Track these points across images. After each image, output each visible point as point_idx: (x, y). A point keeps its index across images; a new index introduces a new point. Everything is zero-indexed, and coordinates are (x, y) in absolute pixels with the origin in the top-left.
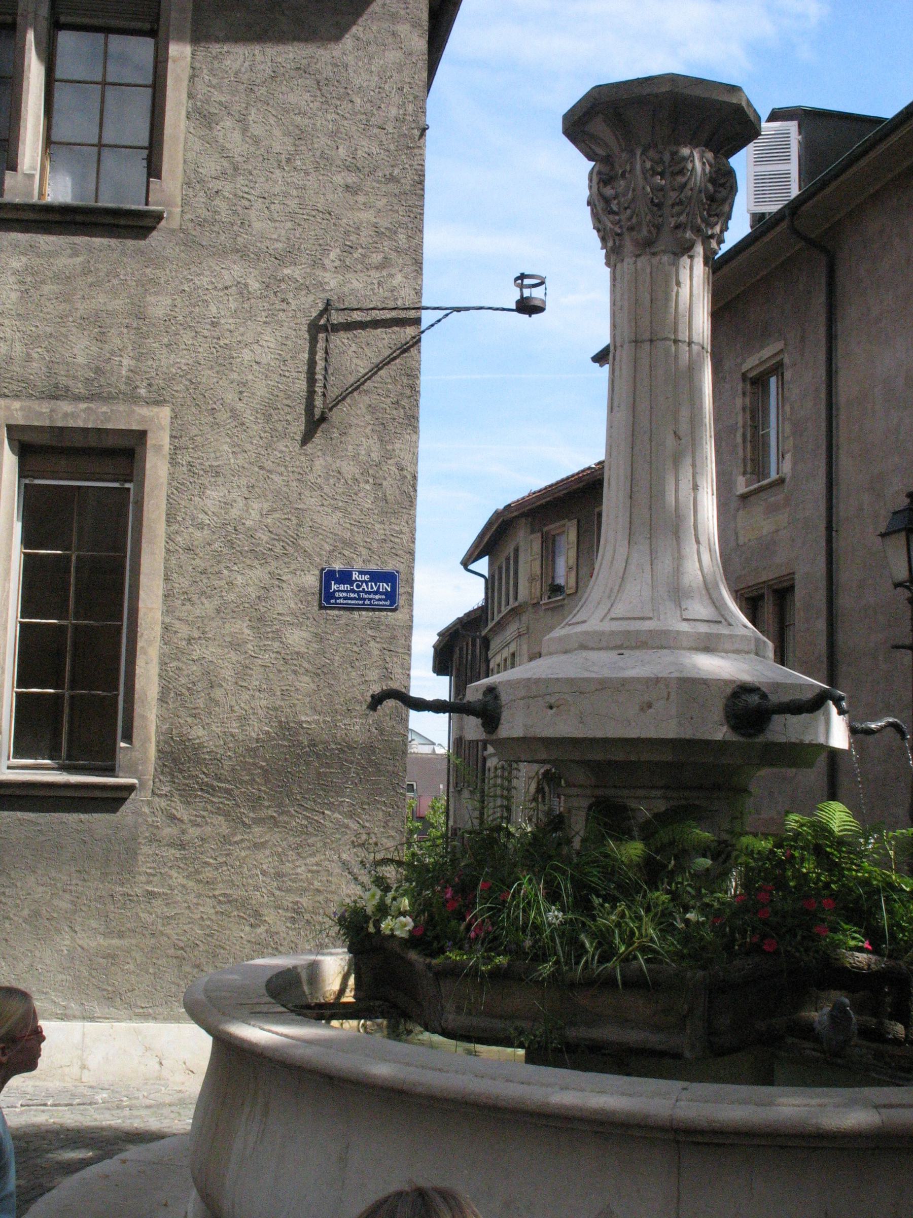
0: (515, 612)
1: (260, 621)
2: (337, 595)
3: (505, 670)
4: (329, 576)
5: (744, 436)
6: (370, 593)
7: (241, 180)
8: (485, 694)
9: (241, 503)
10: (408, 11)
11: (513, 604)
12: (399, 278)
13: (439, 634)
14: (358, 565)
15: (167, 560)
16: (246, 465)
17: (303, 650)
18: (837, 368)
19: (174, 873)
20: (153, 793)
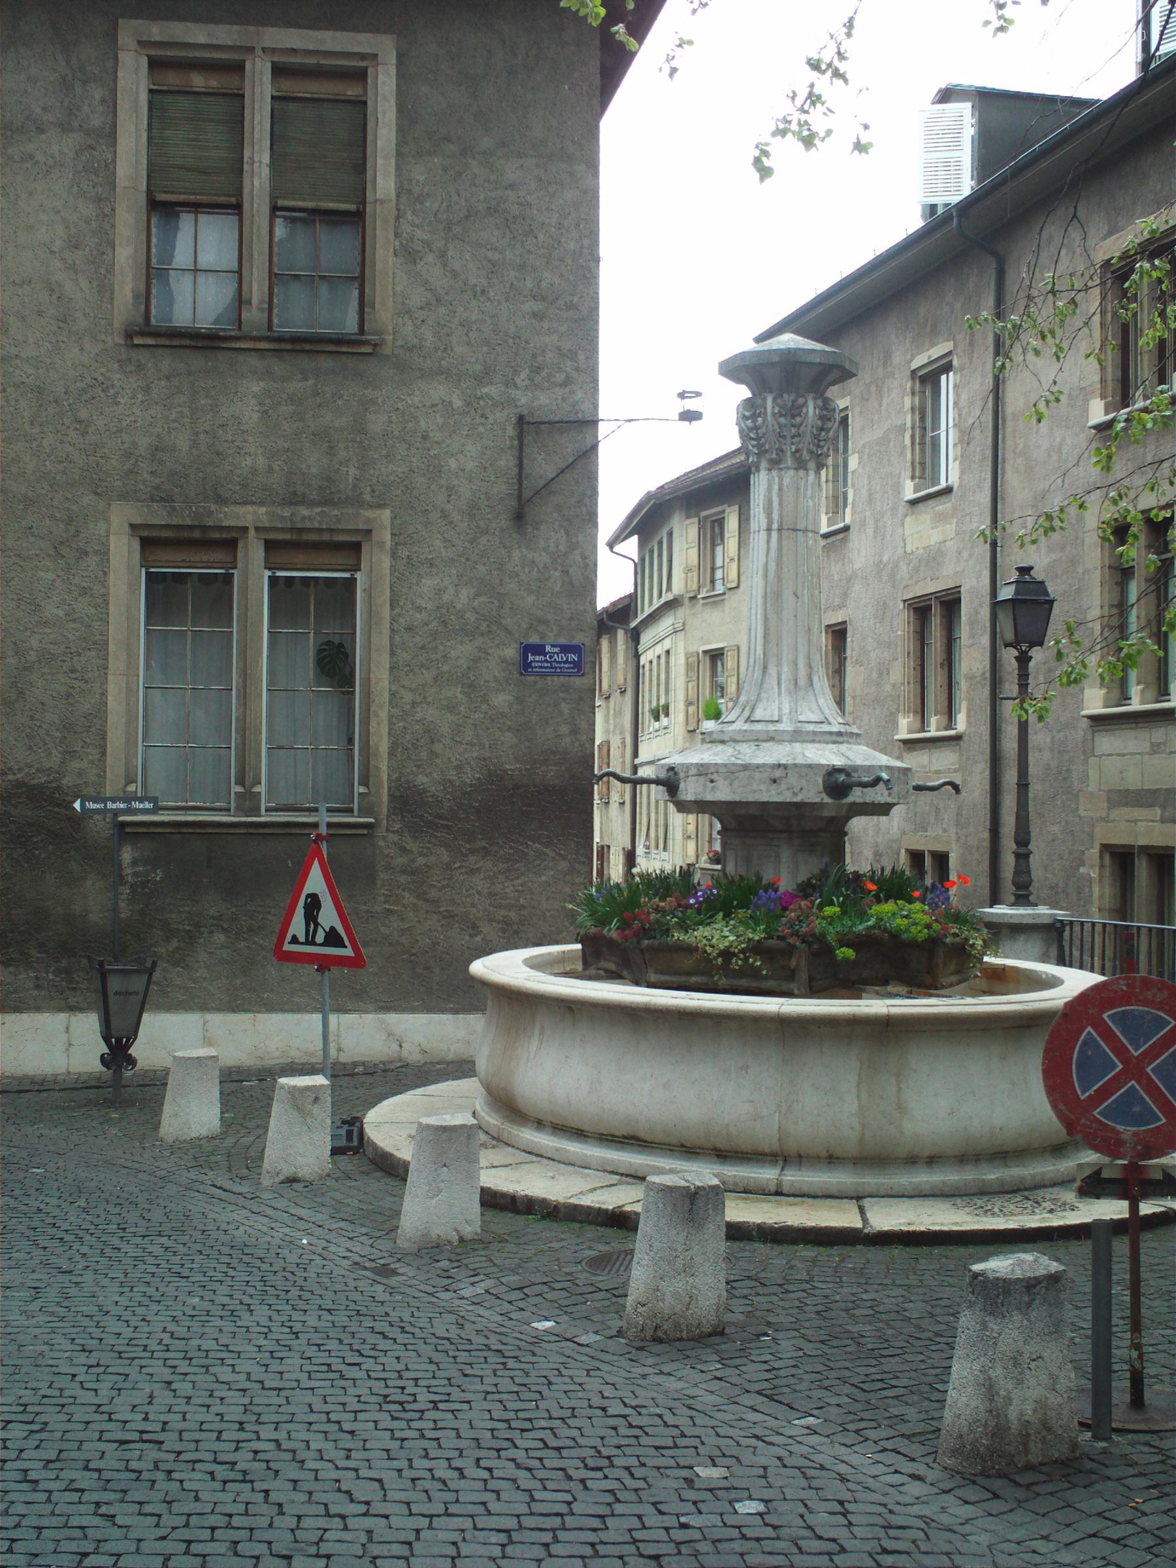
1: (470, 687)
4: (528, 649)
5: (913, 437)
7: (442, 310)
9: (451, 590)
11: (670, 597)
14: (551, 638)
15: (391, 639)
17: (506, 710)
19: (406, 895)
20: (387, 830)
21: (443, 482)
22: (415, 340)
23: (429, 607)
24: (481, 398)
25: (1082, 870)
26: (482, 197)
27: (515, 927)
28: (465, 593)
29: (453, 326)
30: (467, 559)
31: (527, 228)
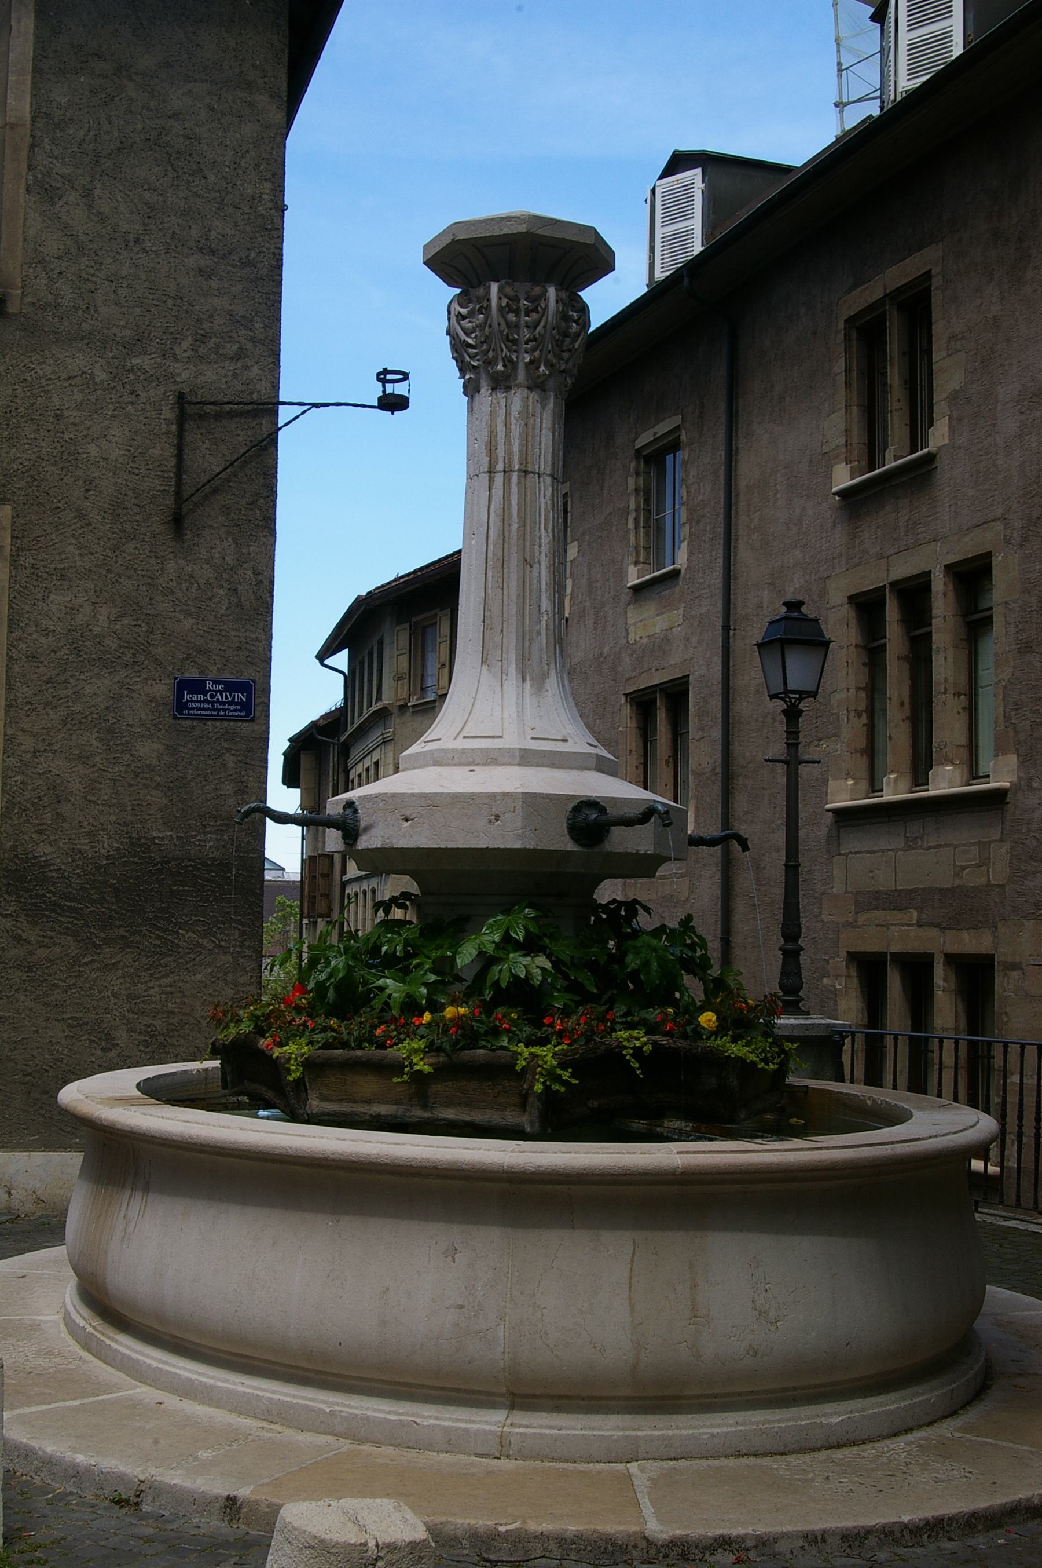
0: (383, 715)
2: (190, 705)
3: (368, 783)
4: (184, 685)
6: (224, 703)
7: (84, 260)
8: (344, 808)
9: (87, 609)
10: (266, 80)
12: (255, 370)
13: (290, 740)
14: (213, 673)
16: (93, 569)
17: (155, 762)
18: (737, 449)
21: (79, 473)
22: (50, 297)
23: (59, 630)
24: (131, 370)
25: (825, 981)
26: (139, 126)
27: (161, 1039)
28: (104, 612)
29: (99, 281)
30: (109, 571)
31: (194, 166)
